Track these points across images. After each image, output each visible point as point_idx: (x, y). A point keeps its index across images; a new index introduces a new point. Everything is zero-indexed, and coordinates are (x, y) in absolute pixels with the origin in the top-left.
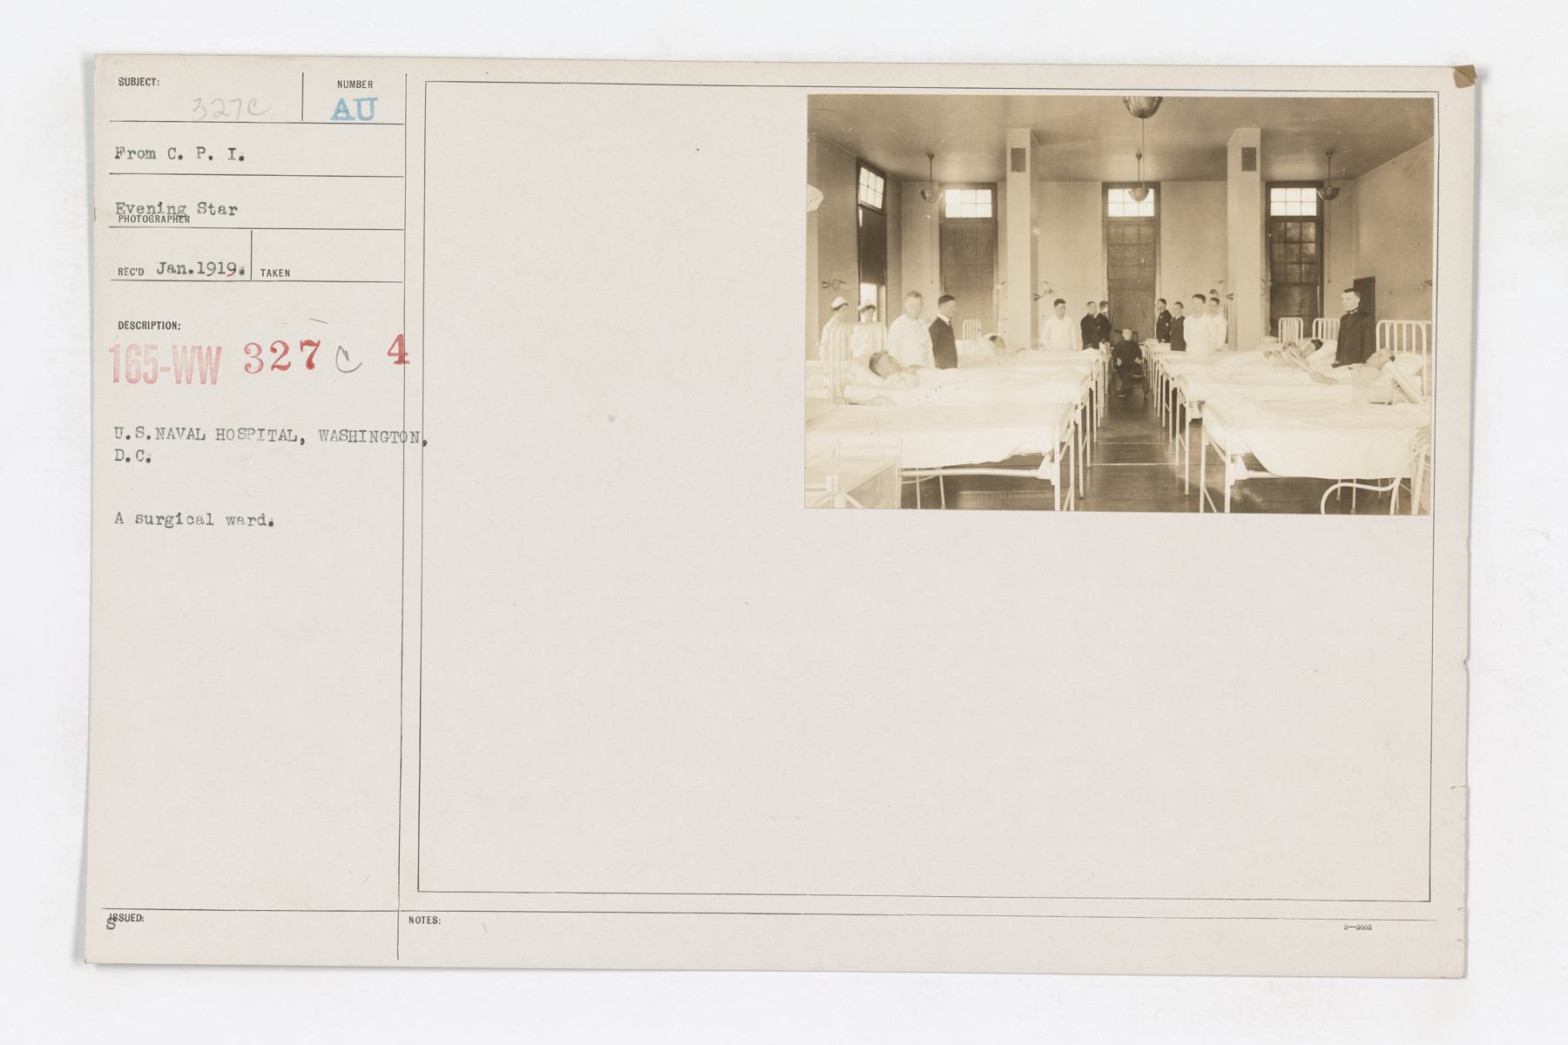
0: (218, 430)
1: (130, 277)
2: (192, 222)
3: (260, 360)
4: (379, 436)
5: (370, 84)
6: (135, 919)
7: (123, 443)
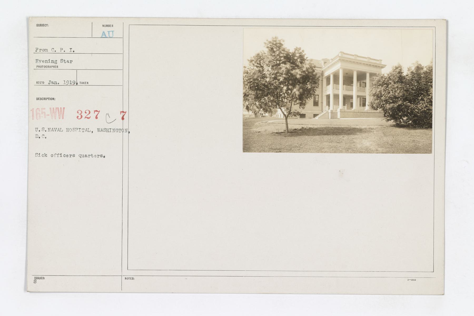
0: (67, 128)
2: (59, 68)
4: (115, 131)
5: (112, 26)
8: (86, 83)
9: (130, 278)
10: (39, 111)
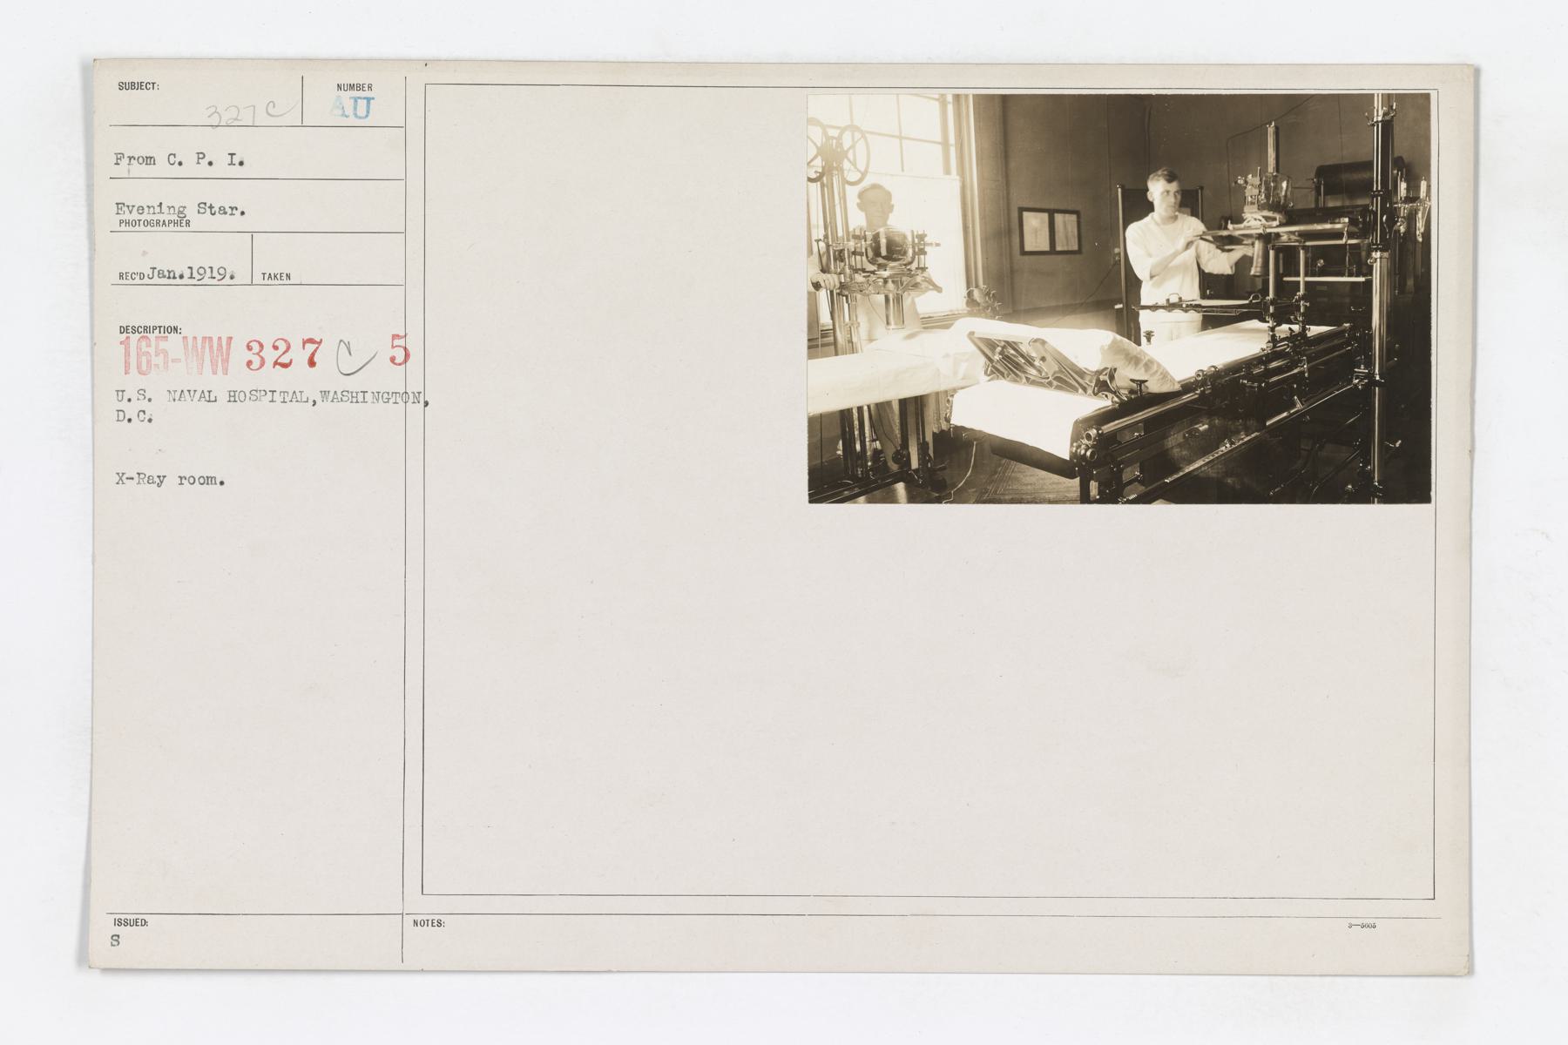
1: (131, 282)
3: (262, 358)
5: (370, 87)
7: (124, 405)
8: (285, 275)
9: (430, 923)
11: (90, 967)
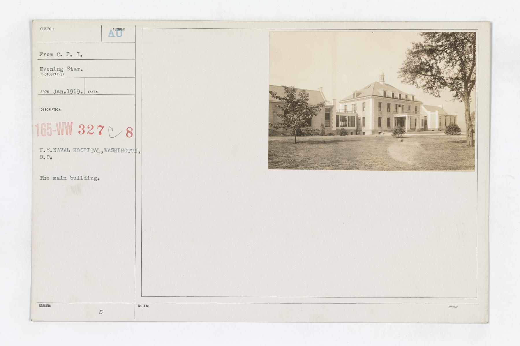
1: (45, 94)
2: (65, 75)
6: (48, 306)
7: (42, 153)
8: (95, 92)
9: (144, 306)
10: (45, 126)
11: (32, 320)
